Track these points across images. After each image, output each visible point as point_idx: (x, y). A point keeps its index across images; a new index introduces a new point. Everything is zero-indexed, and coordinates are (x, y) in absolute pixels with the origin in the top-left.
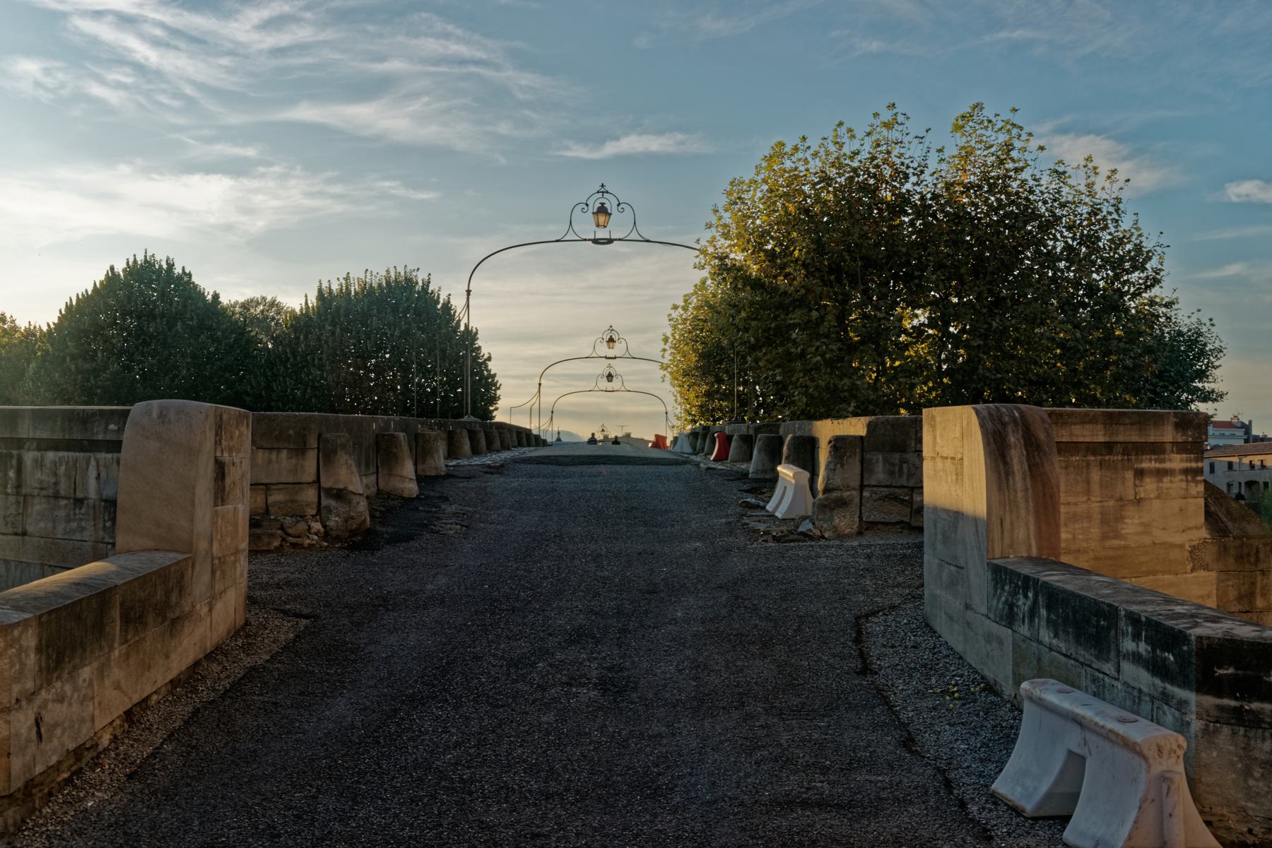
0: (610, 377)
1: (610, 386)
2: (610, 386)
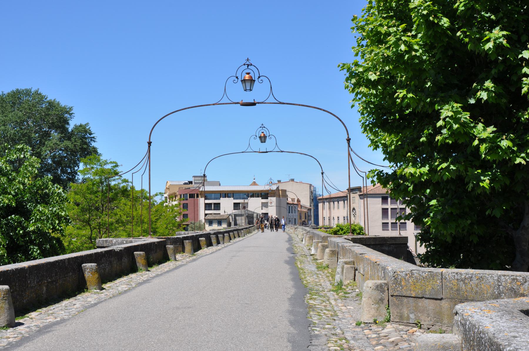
0: (263, 139)
1: (263, 147)
2: (263, 147)
